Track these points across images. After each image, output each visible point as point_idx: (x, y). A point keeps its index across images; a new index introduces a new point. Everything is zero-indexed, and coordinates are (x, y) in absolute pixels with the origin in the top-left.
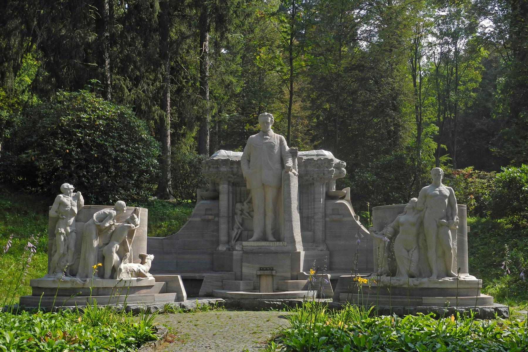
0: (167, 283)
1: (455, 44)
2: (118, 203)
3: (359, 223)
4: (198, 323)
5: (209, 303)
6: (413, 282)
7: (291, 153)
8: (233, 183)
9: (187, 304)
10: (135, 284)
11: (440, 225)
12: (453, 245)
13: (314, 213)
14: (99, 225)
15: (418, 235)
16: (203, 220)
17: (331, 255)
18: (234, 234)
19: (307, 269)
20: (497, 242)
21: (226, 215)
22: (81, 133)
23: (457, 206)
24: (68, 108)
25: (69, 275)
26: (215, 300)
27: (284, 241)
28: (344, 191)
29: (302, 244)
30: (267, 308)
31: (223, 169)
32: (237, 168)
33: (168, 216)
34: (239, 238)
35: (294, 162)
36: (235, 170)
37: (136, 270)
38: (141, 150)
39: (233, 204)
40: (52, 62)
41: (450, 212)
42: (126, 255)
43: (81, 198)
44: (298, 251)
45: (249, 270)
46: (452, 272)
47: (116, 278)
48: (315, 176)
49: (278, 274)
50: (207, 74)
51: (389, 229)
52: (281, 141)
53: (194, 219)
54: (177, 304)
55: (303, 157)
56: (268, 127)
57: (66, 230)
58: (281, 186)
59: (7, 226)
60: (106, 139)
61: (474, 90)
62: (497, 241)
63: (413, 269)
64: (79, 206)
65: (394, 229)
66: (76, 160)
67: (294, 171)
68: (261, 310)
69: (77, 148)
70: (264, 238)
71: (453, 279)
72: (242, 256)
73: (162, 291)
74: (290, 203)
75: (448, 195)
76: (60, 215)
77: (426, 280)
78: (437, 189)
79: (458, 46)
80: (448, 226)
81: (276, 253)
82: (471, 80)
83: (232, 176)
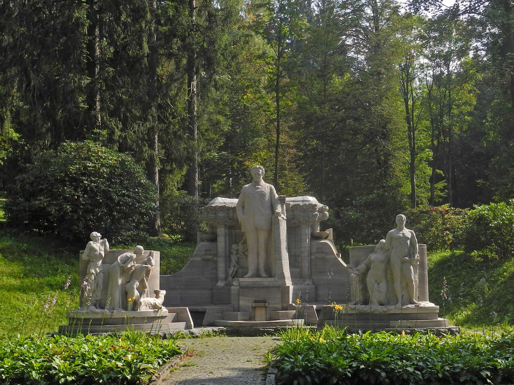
0: (177, 314)
1: (448, 66)
2: (137, 247)
3: (340, 260)
4: (208, 344)
5: (213, 331)
6: (381, 309)
7: (280, 200)
8: (229, 227)
9: (195, 331)
10: (153, 315)
11: (403, 262)
12: (415, 278)
13: (301, 252)
15: (386, 271)
16: (203, 260)
17: (316, 288)
18: (231, 272)
19: (294, 301)
20: (468, 274)
22: (87, 180)
23: (417, 246)
24: (75, 158)
25: (98, 308)
26: (217, 328)
27: (275, 277)
28: (327, 231)
29: (290, 279)
30: (261, 333)
31: (221, 214)
32: (233, 213)
33: (166, 255)
34: (236, 275)
35: (282, 208)
36: (231, 215)
37: (152, 303)
38: (140, 194)
39: (229, 245)
40: (49, 107)
41: (412, 251)
42: (145, 291)
43: (107, 244)
44: (287, 285)
45: (245, 302)
46: (414, 300)
47: (137, 310)
48: (301, 219)
49: (270, 306)
50: (195, 113)
51: (362, 267)
52: (271, 190)
53: (196, 259)
54: (187, 331)
55: (290, 203)
56: (260, 178)
57: (95, 271)
58: (271, 229)
59: (26, 266)
60: (109, 185)
61: (470, 114)
62: (468, 273)
63: (382, 298)
64: (105, 250)
65: (367, 265)
66: (83, 205)
67: (282, 216)
68: (257, 336)
69: (84, 194)
70: (258, 275)
71: (415, 306)
72: (239, 291)
73: (174, 321)
74: (280, 243)
75: (410, 237)
77: (392, 307)
78: (401, 232)
79: (450, 69)
80: (410, 263)
81: (268, 287)
82: (466, 103)
83: (228, 220)
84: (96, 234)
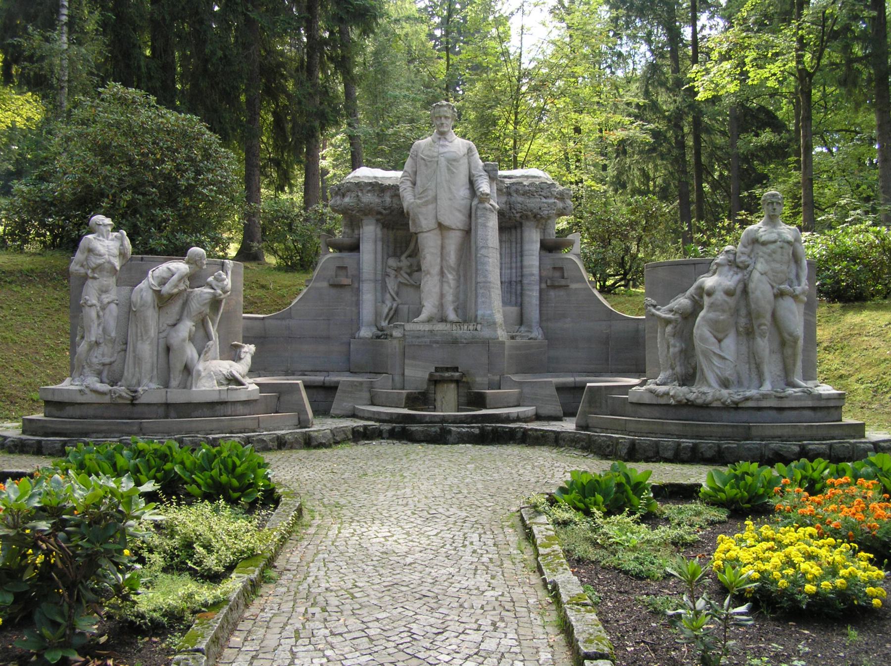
14: (160, 291)
18: (386, 310)
21: (372, 277)
63: (728, 373)
76: (89, 272)
84: (100, 219)
